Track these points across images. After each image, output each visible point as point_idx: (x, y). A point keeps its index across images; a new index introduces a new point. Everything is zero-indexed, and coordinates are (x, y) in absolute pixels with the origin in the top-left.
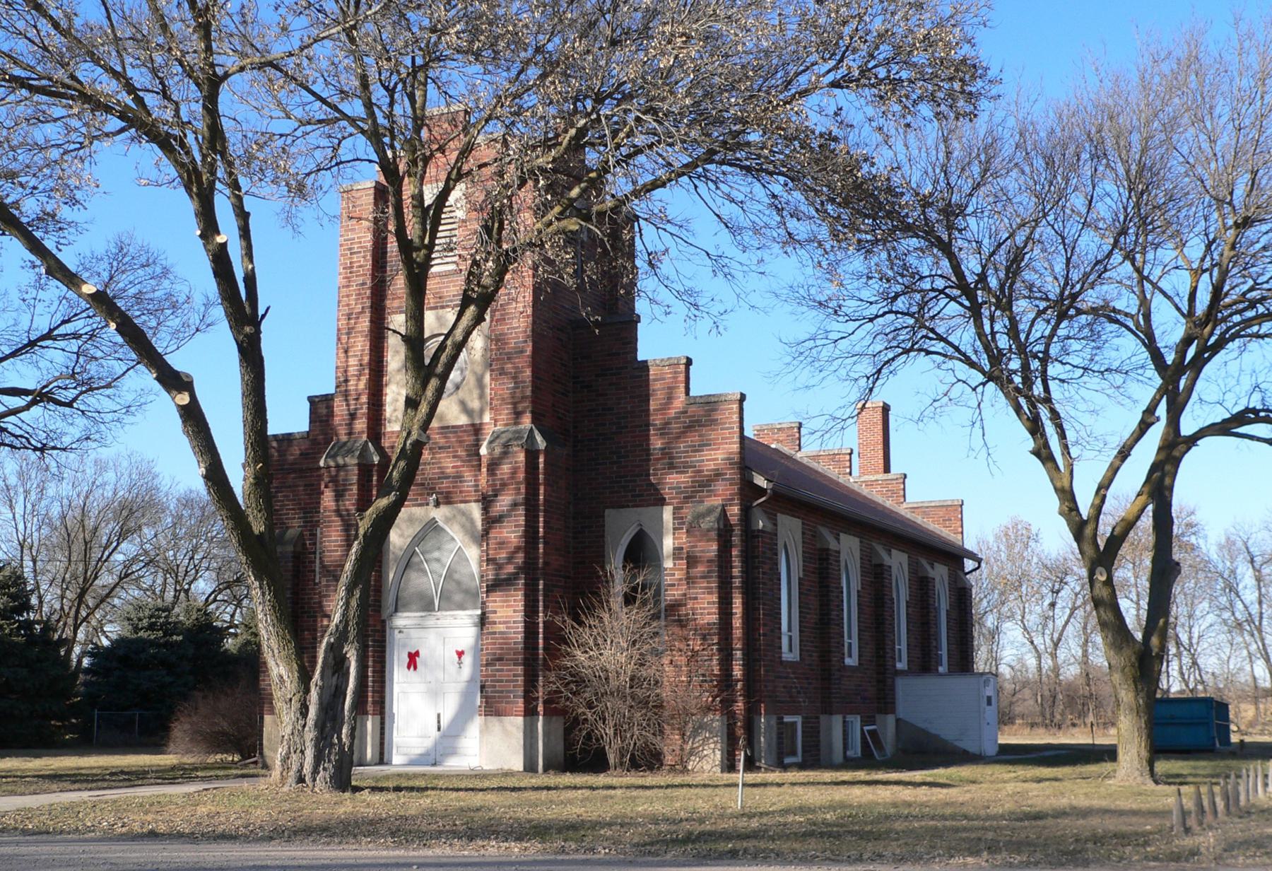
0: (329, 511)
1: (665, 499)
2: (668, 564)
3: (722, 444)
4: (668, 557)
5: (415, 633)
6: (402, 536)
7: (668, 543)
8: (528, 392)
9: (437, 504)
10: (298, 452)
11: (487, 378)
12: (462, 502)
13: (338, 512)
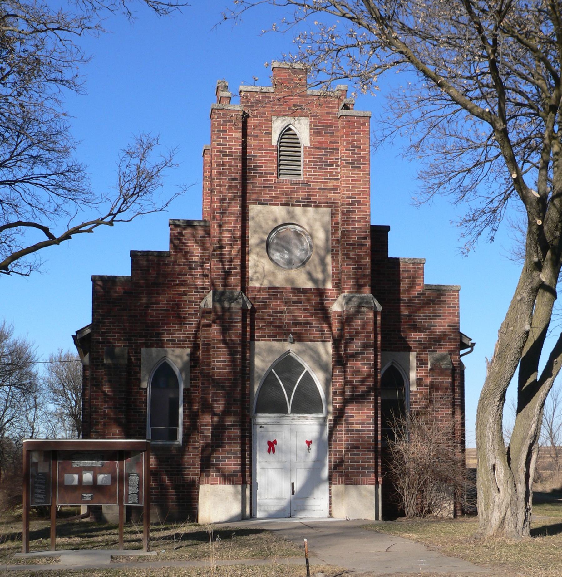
0: (218, 340)
1: (411, 348)
2: (413, 388)
4: (413, 384)
5: (270, 428)
6: (263, 361)
7: (413, 376)
8: (368, 272)
9: (293, 342)
10: (122, 291)
11: (329, 259)
12: (311, 341)
13: (224, 341)
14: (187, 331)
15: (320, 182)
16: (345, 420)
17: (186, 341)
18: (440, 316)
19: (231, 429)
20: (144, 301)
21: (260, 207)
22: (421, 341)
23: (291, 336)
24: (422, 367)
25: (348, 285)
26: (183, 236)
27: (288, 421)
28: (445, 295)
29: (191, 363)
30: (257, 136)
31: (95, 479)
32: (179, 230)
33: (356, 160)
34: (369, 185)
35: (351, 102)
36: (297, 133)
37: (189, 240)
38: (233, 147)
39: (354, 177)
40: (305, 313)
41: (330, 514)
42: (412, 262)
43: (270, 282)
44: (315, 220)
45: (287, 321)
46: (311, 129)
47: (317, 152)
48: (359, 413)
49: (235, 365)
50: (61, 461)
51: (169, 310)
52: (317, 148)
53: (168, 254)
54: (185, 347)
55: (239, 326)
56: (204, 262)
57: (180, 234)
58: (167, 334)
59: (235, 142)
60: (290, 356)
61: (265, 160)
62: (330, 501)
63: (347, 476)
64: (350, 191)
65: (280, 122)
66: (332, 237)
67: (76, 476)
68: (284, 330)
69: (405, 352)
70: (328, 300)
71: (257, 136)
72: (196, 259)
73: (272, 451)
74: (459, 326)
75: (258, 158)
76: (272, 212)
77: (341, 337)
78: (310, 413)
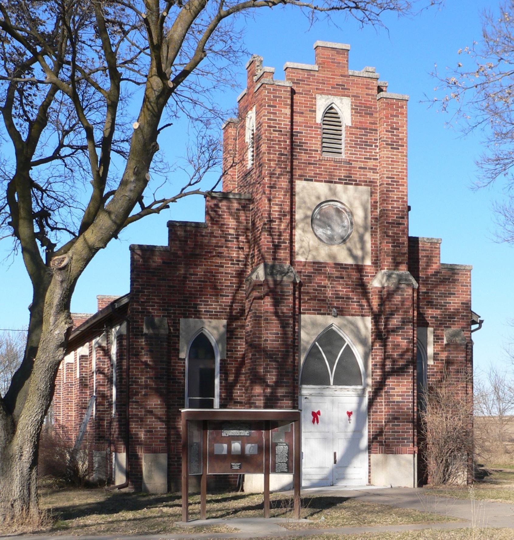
1: (428, 323)
2: (431, 362)
3: (461, 294)
4: (430, 358)
5: (313, 399)
6: (308, 334)
11: (368, 237)
12: (353, 315)
13: (276, 314)
14: (223, 302)
15: (361, 161)
16: (386, 392)
17: (222, 312)
18: (455, 294)
19: (283, 400)
20: (182, 272)
21: (304, 183)
22: (437, 317)
23: (334, 310)
24: (438, 342)
25: (387, 261)
26: (220, 208)
27: (331, 393)
28: (458, 274)
29: (227, 334)
30: (302, 113)
31: (243, 449)
32: (215, 202)
33: (395, 142)
34: (407, 166)
35: (385, 85)
36: (339, 112)
37: (224, 212)
38: (283, 123)
39: (393, 158)
40: (346, 288)
41: (370, 482)
42: (431, 241)
43: (314, 257)
44: (355, 198)
45: (330, 295)
46: (352, 109)
47: (358, 131)
48: (399, 385)
49: (287, 338)
50: (211, 431)
51: (206, 282)
52: (357, 128)
53: (204, 226)
54: (222, 319)
55: (291, 298)
56: (238, 235)
57: (217, 206)
58: (205, 305)
59: (284, 117)
60: (332, 329)
61: (310, 137)
62: (370, 469)
63: (387, 446)
64: (390, 171)
65: (324, 100)
66: (372, 215)
67: (225, 446)
68: (327, 304)
69: (424, 328)
70: (368, 276)
71: (302, 113)
72: (231, 231)
73: (316, 421)
74: (471, 304)
75: (303, 134)
76: (315, 189)
77: (381, 312)
78: (350, 385)
